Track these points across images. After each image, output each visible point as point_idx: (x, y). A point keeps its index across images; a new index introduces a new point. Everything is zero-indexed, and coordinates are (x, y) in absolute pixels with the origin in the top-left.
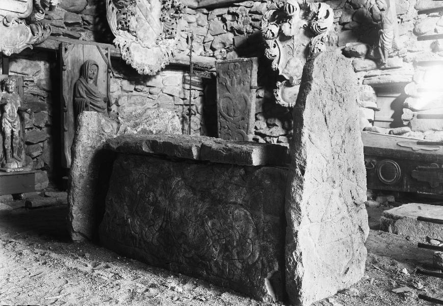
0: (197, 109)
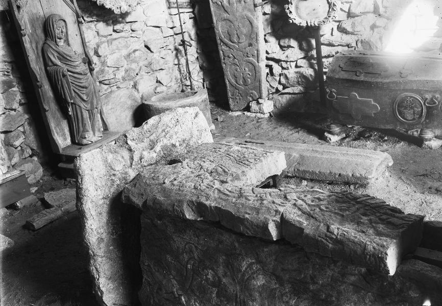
0: (190, 36)
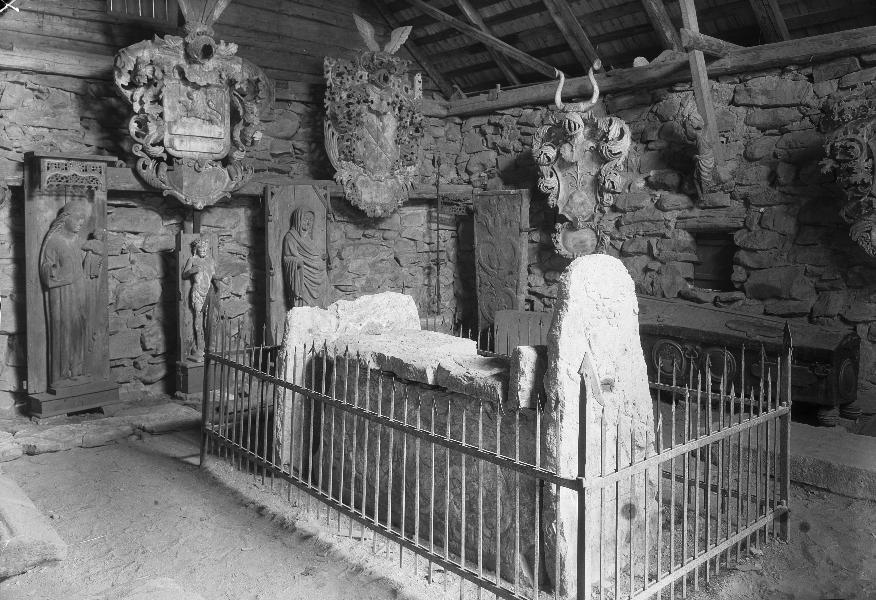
0: (448, 257)
